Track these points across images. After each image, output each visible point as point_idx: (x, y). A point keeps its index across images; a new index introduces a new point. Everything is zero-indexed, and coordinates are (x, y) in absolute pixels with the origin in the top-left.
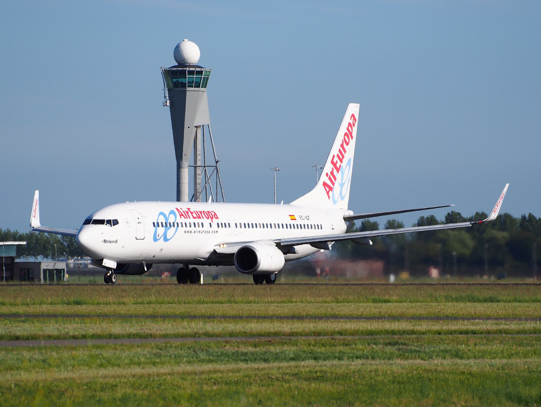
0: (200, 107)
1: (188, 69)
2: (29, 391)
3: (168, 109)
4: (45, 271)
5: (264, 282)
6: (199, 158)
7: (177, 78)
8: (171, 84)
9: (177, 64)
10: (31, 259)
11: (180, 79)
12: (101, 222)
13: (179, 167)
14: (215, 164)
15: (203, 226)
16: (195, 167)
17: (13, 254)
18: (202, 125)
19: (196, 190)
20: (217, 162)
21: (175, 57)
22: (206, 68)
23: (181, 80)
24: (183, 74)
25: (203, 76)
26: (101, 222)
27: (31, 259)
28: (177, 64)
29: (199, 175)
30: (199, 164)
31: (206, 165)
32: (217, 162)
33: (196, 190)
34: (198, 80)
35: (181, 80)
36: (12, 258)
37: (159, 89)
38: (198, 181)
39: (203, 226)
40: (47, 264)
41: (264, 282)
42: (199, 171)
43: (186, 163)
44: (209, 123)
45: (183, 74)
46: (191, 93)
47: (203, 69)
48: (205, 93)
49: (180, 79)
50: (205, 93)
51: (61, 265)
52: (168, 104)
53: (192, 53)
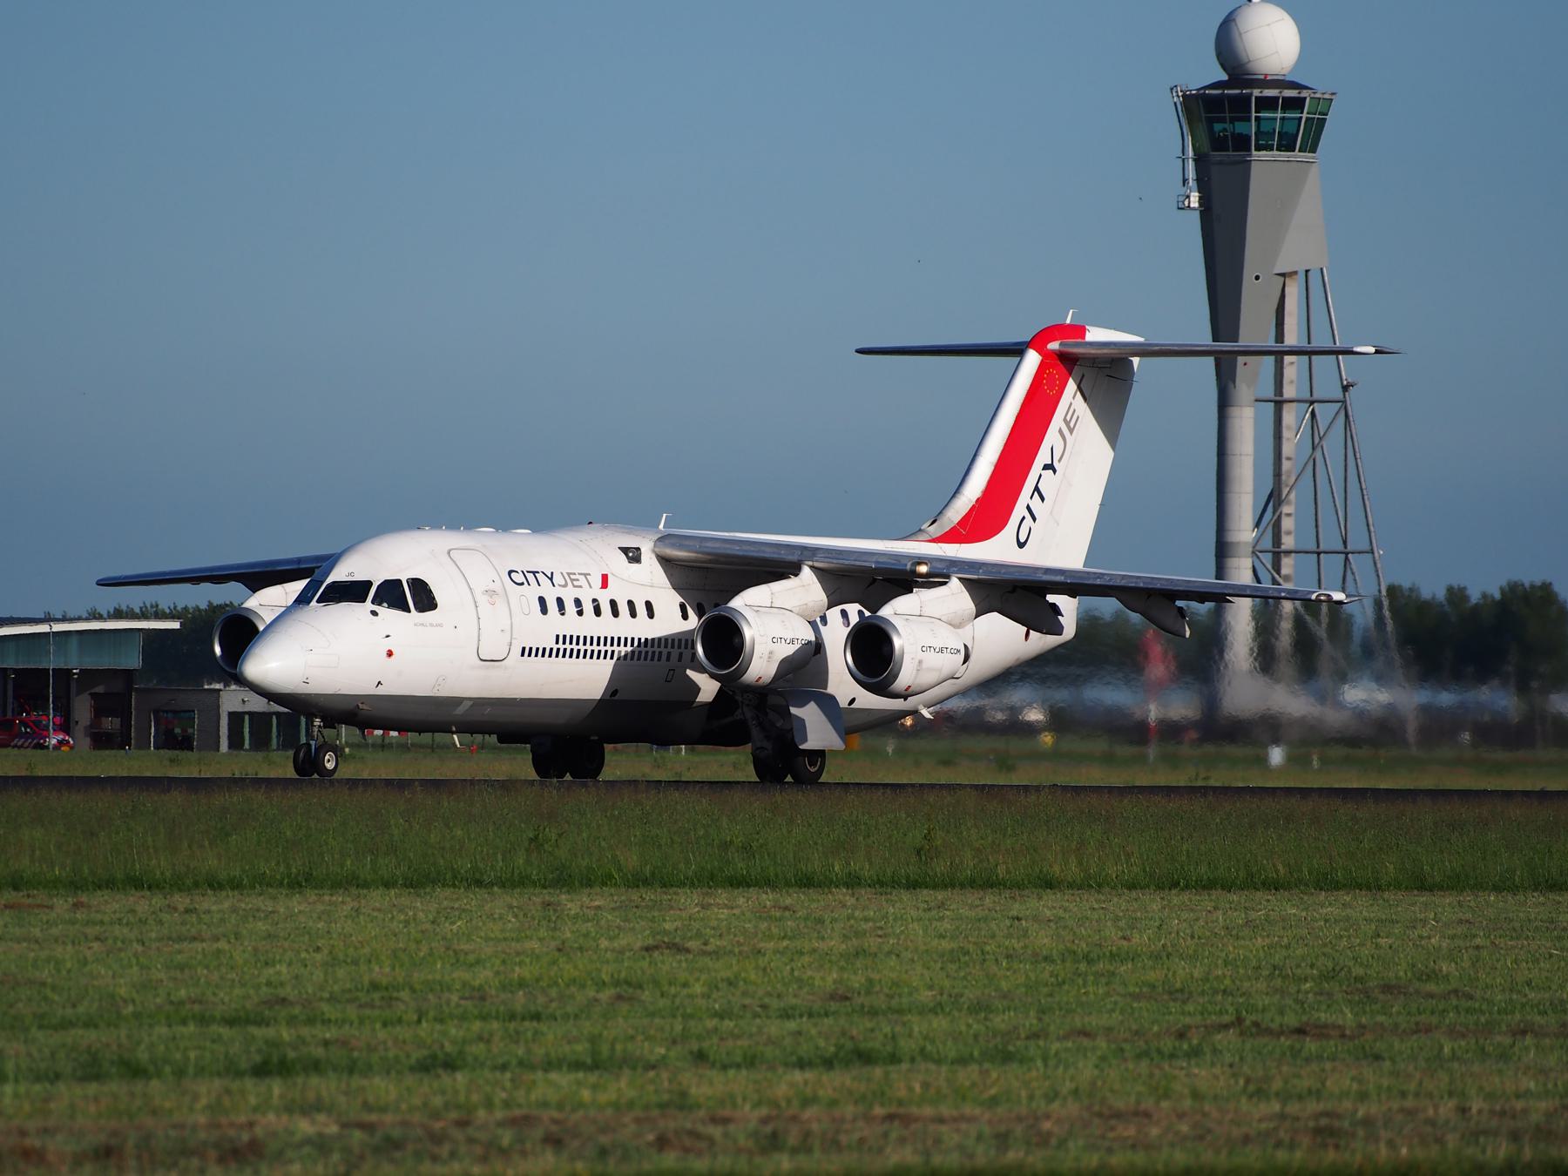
0: (1300, 214)
1: (1256, 92)
2: (388, 1073)
3: (1194, 222)
4: (235, 718)
5: (789, 779)
7: (1223, 120)
8: (1206, 147)
9: (1225, 77)
11: (1236, 123)
12: (353, 592)
14: (1339, 394)
15: (651, 614)
16: (1279, 404)
17: (132, 660)
18: (1301, 269)
19: (1278, 474)
20: (1345, 388)
21: (1219, 55)
22: (1319, 83)
23: (1240, 127)
24: (1240, 106)
25: (1305, 115)
26: (353, 592)
28: (1225, 77)
29: (1289, 428)
30: (1289, 392)
31: (1316, 396)
32: (1345, 388)
33: (1278, 474)
34: (1290, 128)
35: (1240, 127)
36: (128, 674)
38: (1288, 449)
39: (651, 614)
41: (789, 779)
42: (1289, 416)
45: (1240, 106)
46: (1265, 166)
47: (1305, 94)
49: (1236, 123)
50: (1314, 169)
52: (1194, 201)
53: (1274, 42)
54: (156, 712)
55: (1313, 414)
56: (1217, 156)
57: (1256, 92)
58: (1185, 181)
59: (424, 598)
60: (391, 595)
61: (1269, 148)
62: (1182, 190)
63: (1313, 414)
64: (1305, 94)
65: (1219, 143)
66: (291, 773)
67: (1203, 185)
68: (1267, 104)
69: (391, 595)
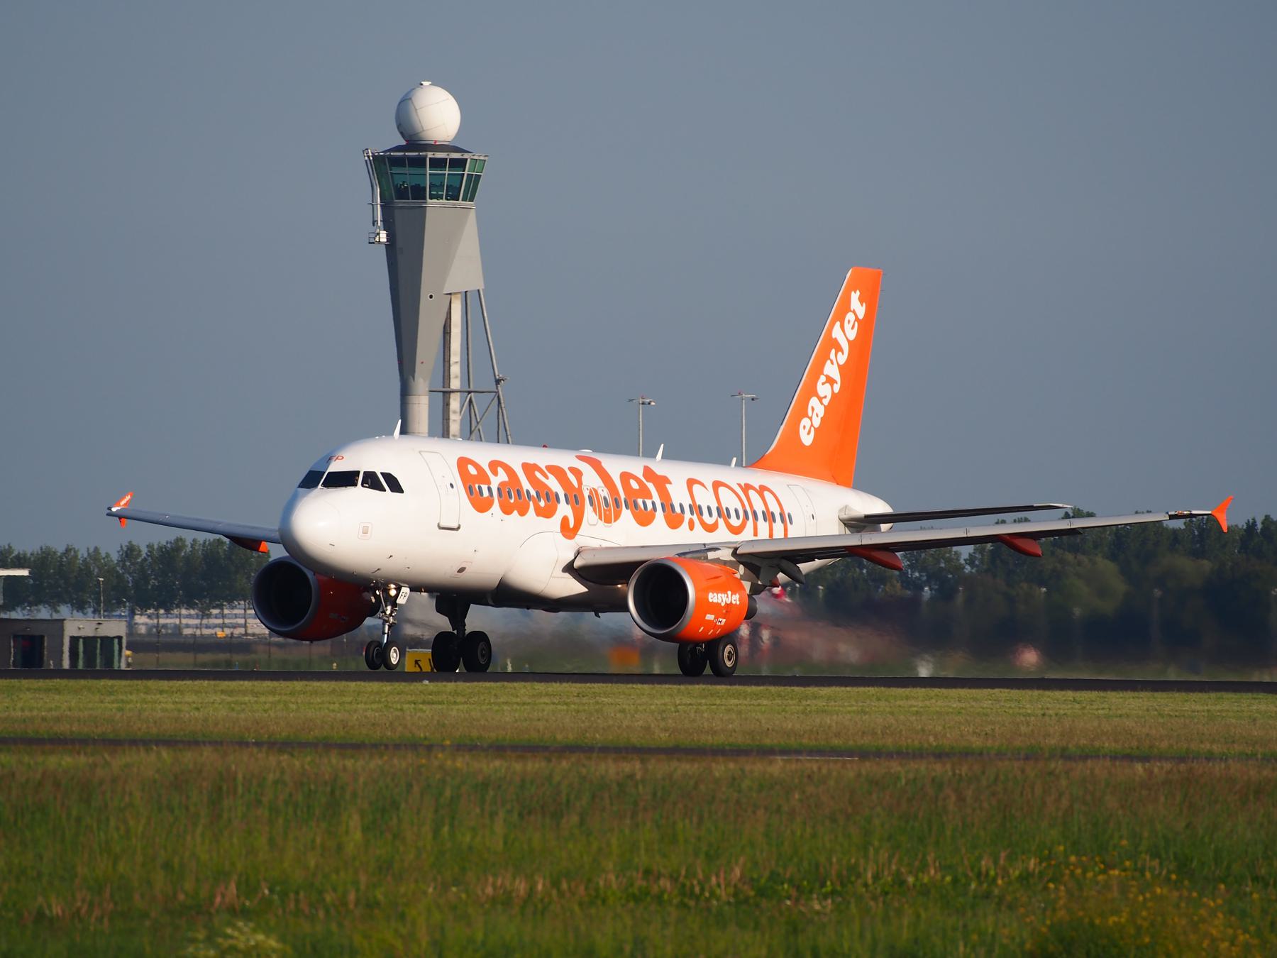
0: (458, 251)
1: (430, 155)
4: (74, 640)
6: (455, 370)
9: (404, 143)
10: (44, 613)
13: (406, 392)
16: (447, 394)
20: (498, 382)
21: (399, 126)
26: (345, 479)
27: (44, 613)
28: (404, 143)
29: (455, 412)
30: (455, 384)
31: (472, 388)
32: (498, 382)
37: (363, 198)
40: (78, 625)
42: (455, 403)
43: (421, 384)
44: (481, 287)
46: (436, 209)
47: (466, 156)
48: (472, 214)
49: (411, 177)
51: (114, 627)
52: (383, 237)
53: (440, 115)
54: (15, 637)
55: (471, 401)
56: (400, 203)
57: (430, 155)
58: (374, 222)
59: (395, 486)
60: (372, 481)
61: (439, 197)
62: (372, 229)
63: (471, 401)
64: (466, 156)
65: (401, 193)
66: (364, 667)
67: (388, 225)
68: (437, 163)
69: (372, 481)
